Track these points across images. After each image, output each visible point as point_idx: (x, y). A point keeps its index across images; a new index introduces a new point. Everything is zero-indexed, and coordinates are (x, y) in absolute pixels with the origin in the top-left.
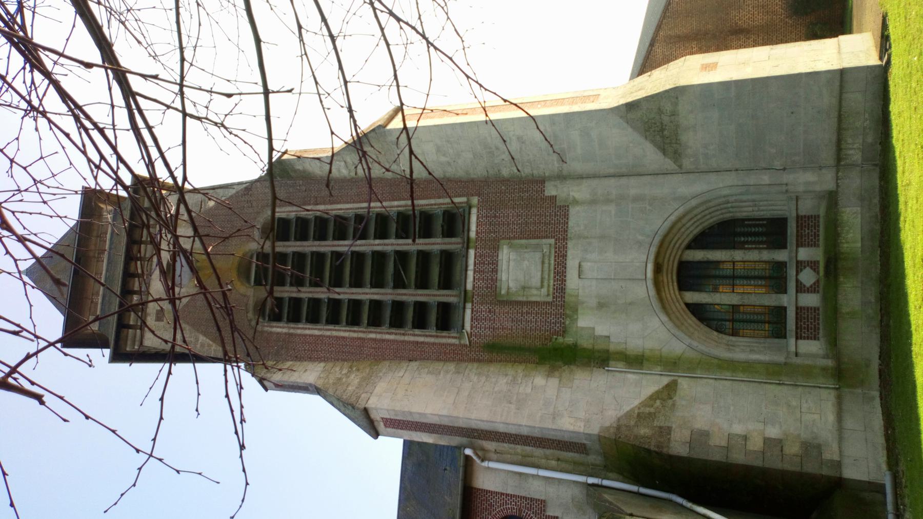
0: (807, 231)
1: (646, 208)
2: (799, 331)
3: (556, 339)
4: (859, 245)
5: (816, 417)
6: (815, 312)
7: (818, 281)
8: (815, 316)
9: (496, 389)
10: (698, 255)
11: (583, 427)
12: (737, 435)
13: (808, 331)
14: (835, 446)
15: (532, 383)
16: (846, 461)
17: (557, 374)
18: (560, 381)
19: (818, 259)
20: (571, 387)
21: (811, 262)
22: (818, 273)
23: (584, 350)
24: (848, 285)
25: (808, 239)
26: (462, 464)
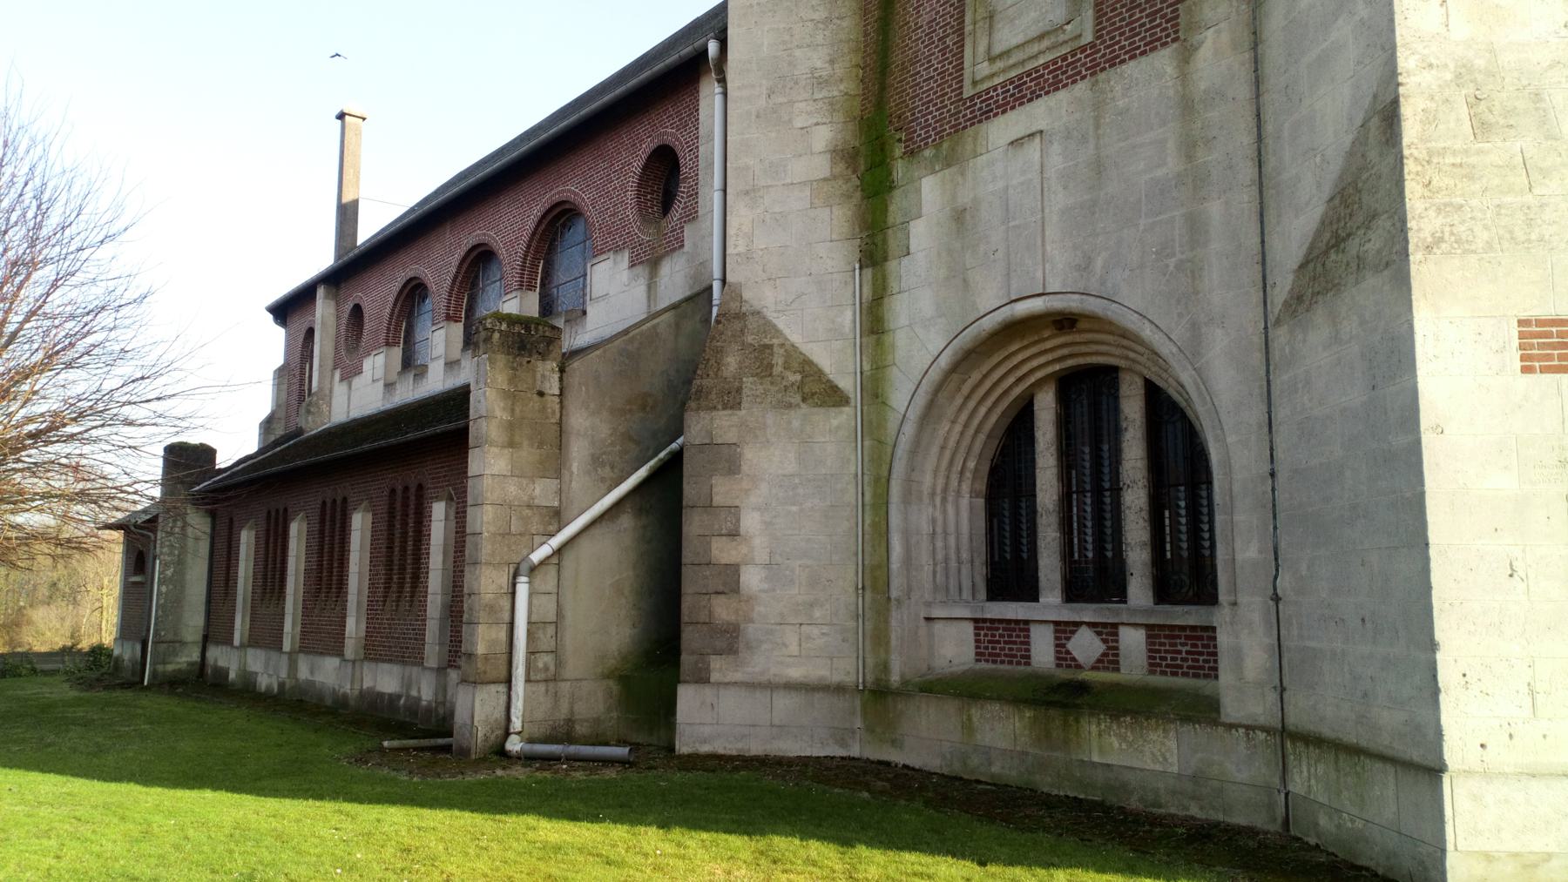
0: (1184, 649)
1: (1174, 255)
2: (988, 625)
3: (900, 140)
4: (1096, 758)
5: (793, 648)
6: (1022, 657)
7: (1079, 667)
8: (1016, 656)
9: (798, 53)
10: (1132, 408)
11: (735, 252)
12: (738, 520)
13: (989, 642)
14: (738, 676)
15: (817, 124)
16: (707, 692)
17: (841, 167)
18: (825, 180)
19: (1122, 671)
20: (813, 206)
21: (1117, 655)
22: (1094, 668)
23: (885, 211)
24: (1017, 724)
25: (1166, 652)
26: (682, 53)
